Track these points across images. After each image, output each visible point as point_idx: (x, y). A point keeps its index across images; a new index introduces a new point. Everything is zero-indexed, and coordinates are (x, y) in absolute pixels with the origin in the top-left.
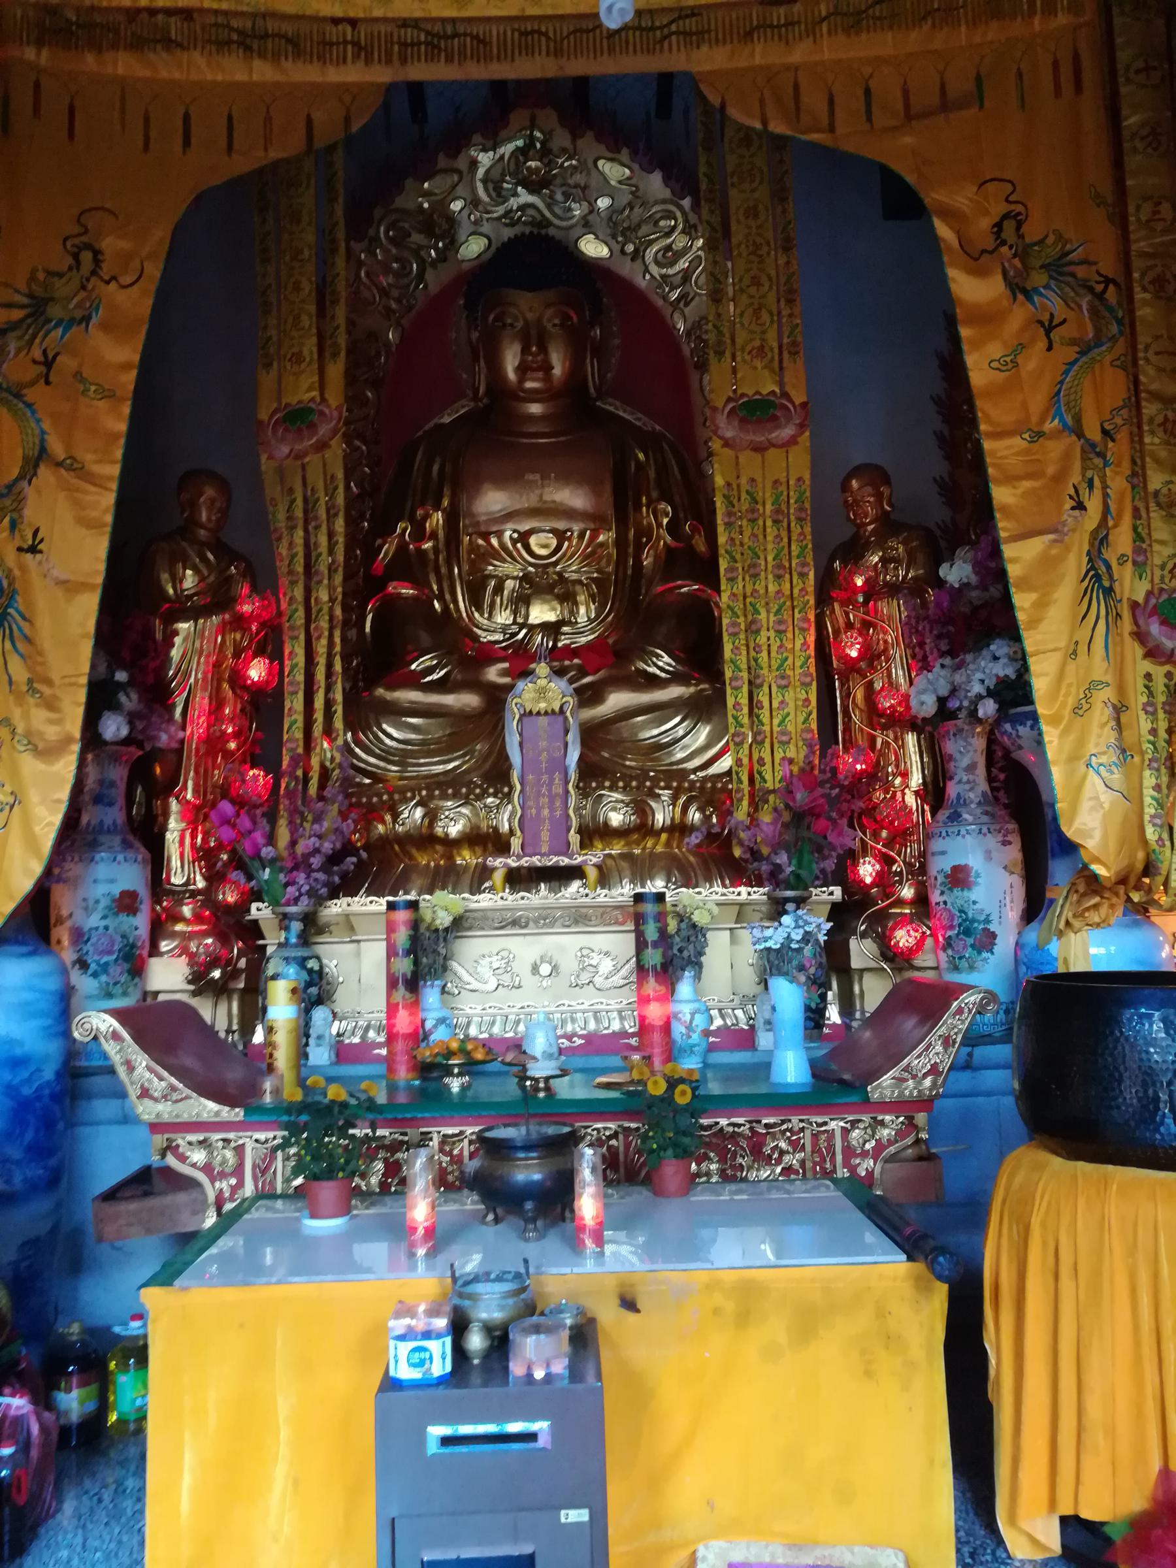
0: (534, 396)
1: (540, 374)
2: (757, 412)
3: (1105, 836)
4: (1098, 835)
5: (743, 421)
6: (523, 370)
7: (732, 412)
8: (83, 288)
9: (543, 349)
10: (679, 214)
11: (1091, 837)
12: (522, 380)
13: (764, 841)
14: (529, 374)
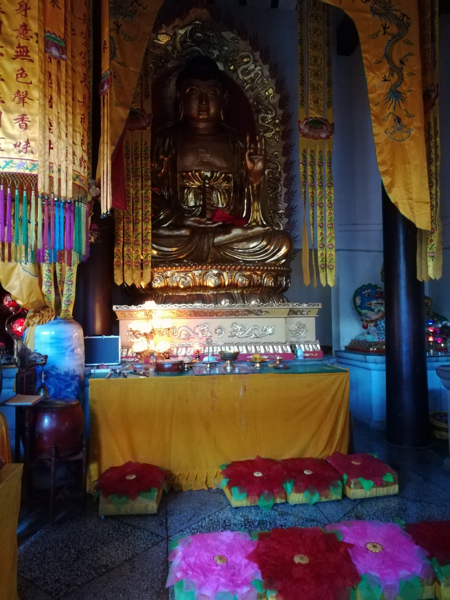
0: (203, 120)
1: (205, 113)
2: (316, 124)
3: (21, 290)
4: (17, 289)
5: (311, 127)
6: (199, 111)
7: (307, 124)
8: (132, 6)
9: (208, 103)
10: (251, 57)
11: (14, 289)
12: (199, 115)
13: (157, 280)
14: (201, 113)
